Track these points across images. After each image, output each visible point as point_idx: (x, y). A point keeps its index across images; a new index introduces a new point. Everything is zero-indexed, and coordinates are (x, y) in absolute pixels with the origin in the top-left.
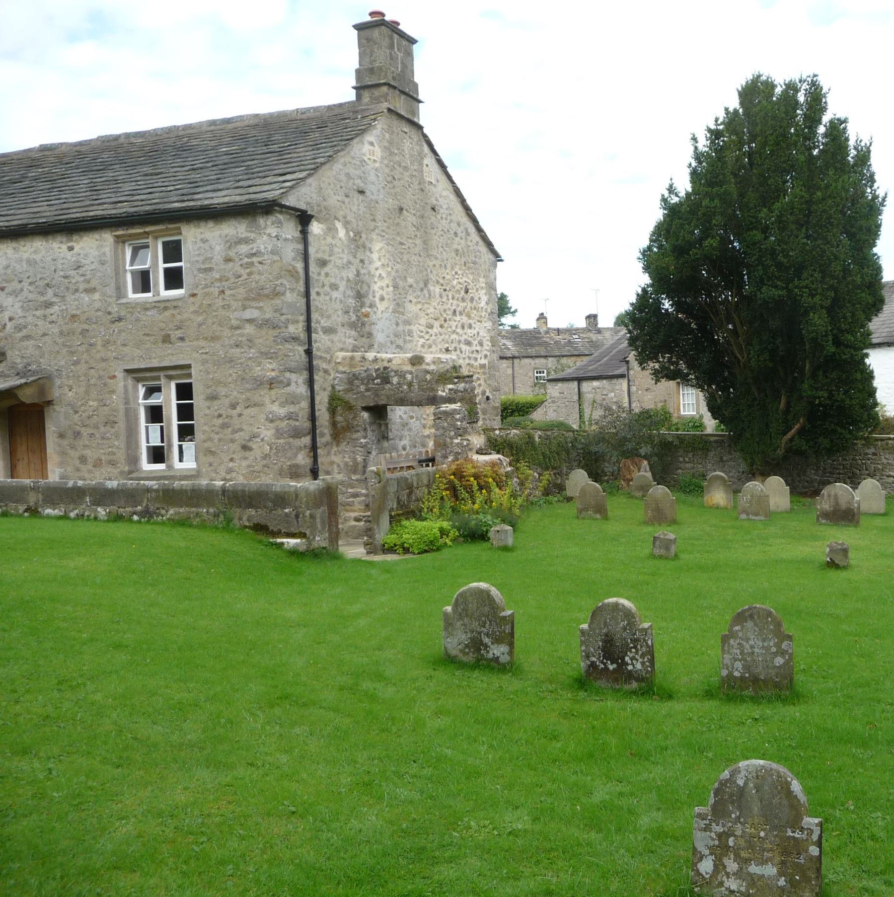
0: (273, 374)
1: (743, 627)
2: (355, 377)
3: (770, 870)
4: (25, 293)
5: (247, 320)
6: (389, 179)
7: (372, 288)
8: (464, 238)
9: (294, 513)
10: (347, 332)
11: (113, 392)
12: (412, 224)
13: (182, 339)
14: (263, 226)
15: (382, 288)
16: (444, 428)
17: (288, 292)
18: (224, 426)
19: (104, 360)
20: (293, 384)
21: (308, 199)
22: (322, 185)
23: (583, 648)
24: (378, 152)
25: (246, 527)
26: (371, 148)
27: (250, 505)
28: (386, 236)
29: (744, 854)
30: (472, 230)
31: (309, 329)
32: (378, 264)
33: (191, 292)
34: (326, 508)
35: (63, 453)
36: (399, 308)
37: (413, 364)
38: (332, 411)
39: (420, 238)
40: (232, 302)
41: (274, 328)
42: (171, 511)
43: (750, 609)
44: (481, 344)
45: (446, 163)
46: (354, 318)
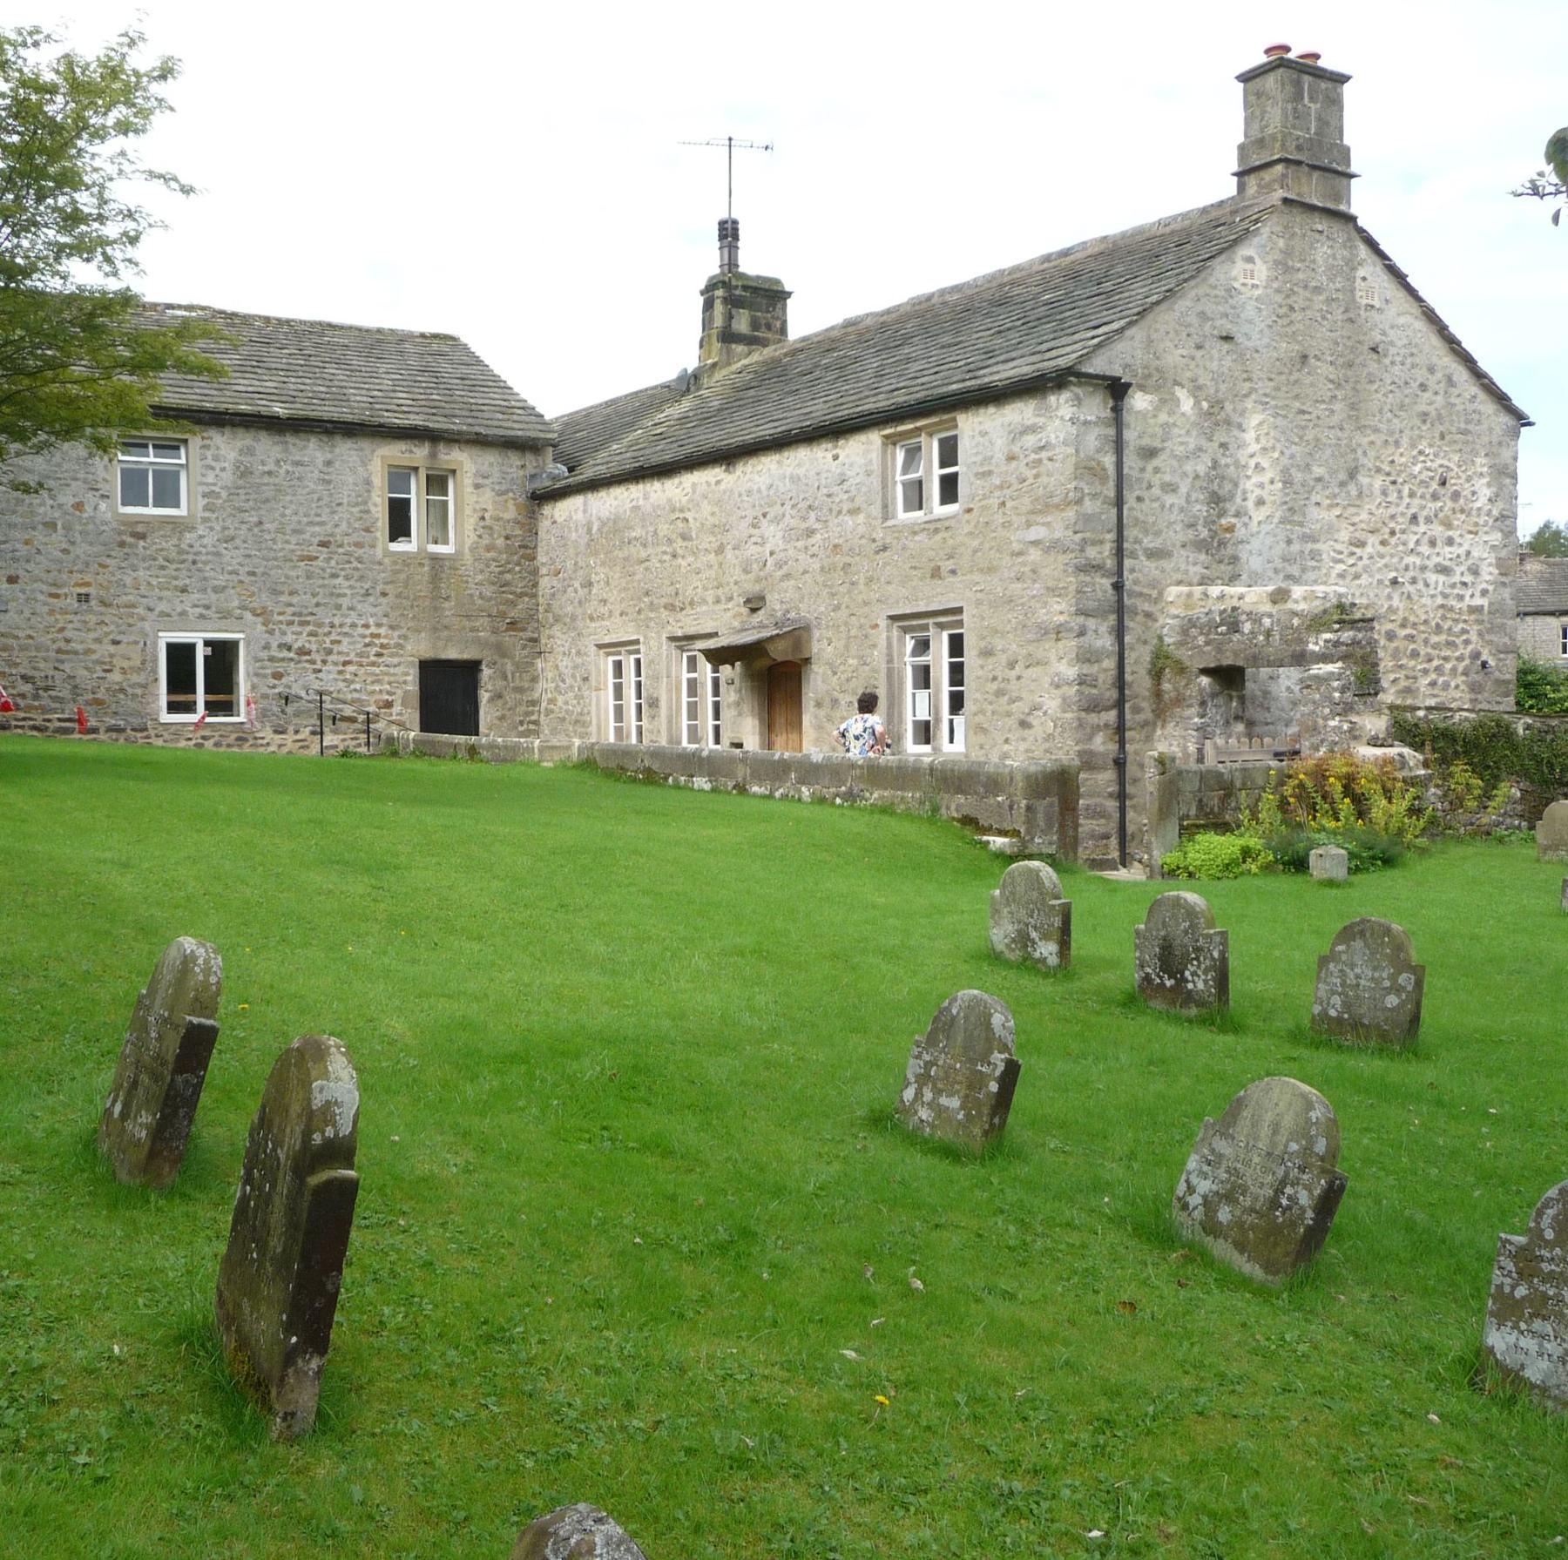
0: (1062, 618)
1: (1349, 947)
2: (1192, 623)
3: (955, 1103)
4: (787, 519)
5: (1031, 542)
6: (1284, 310)
7: (1241, 487)
8: (1442, 392)
9: (1008, 802)
10: (1191, 555)
11: (874, 646)
12: (1327, 378)
13: (953, 572)
14: (1054, 406)
15: (1261, 486)
16: (1314, 703)
17: (1087, 499)
18: (1000, 693)
19: (866, 603)
20: (1090, 633)
21: (1129, 360)
22: (1154, 336)
23: (1138, 954)
24: (1262, 271)
25: (954, 819)
26: (1249, 266)
27: (960, 790)
28: (1273, 403)
29: (940, 1086)
30: (1461, 374)
31: (1119, 553)
32: (1254, 447)
33: (966, 506)
34: (1055, 800)
35: (819, 728)
36: (1292, 513)
37: (1274, 602)
38: (1157, 675)
39: (1344, 400)
40: (1014, 518)
41: (1064, 552)
42: (875, 795)
43: (1363, 921)
44: (1475, 571)
45: (1404, 269)
46: (1205, 533)
